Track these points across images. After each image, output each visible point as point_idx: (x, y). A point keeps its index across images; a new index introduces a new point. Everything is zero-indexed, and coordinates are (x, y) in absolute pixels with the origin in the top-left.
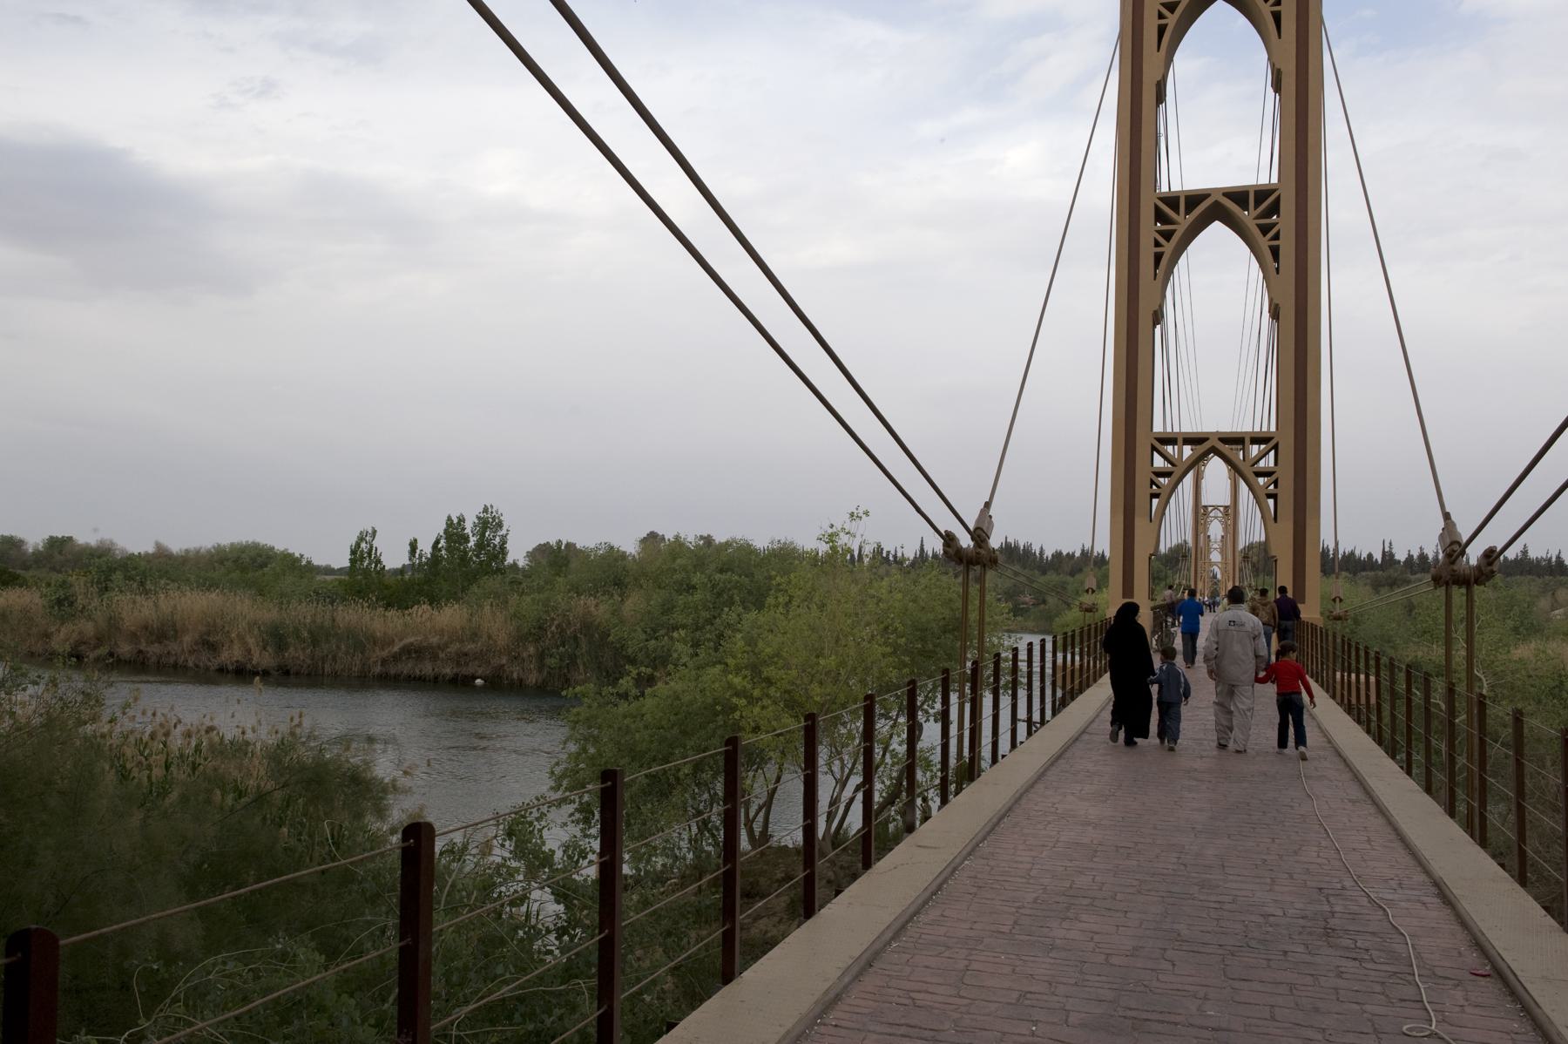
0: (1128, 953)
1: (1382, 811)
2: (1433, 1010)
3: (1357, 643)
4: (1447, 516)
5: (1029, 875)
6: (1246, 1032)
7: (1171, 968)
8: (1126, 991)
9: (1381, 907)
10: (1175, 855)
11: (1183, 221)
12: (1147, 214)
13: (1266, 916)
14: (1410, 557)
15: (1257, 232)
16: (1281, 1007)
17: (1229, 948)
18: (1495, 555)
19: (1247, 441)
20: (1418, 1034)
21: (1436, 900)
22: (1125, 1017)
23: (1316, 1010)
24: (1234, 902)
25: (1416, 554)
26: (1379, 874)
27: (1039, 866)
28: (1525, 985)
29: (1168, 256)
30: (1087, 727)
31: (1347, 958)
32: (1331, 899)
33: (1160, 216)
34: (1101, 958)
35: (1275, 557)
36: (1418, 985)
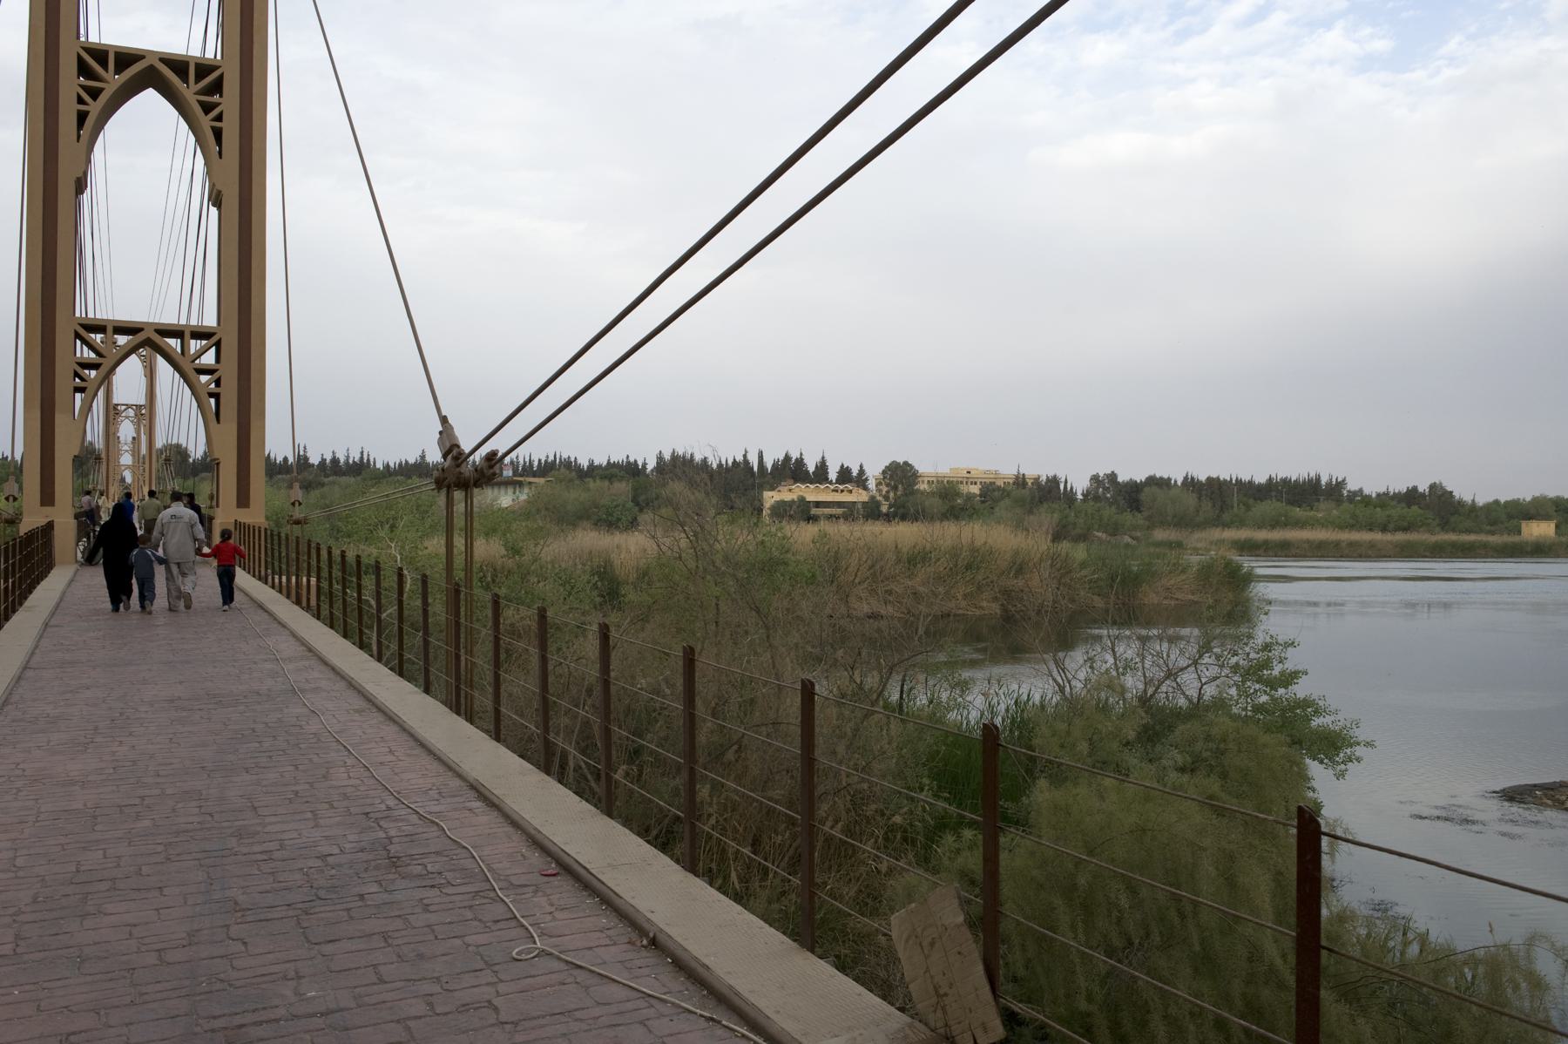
0: (185, 943)
1: (391, 718)
2: (530, 925)
3: (318, 544)
4: (444, 420)
5: (15, 866)
6: (359, 1006)
7: (243, 948)
8: (200, 994)
9: (433, 822)
10: (194, 804)
11: (113, 81)
12: (68, 67)
13: (323, 857)
14: (323, 461)
15: (198, 110)
16: (385, 964)
17: (300, 906)
18: (463, 457)
19: (187, 335)
20: (529, 956)
21: (479, 804)
22: (213, 1031)
23: (421, 956)
24: (282, 847)
25: (328, 458)
26: (416, 787)
27: (25, 852)
28: (599, 877)
29: (94, 118)
30: (28, 662)
31: (425, 887)
32: (382, 823)
33: (84, 70)
34: (152, 959)
35: (218, 459)
36: (503, 901)
